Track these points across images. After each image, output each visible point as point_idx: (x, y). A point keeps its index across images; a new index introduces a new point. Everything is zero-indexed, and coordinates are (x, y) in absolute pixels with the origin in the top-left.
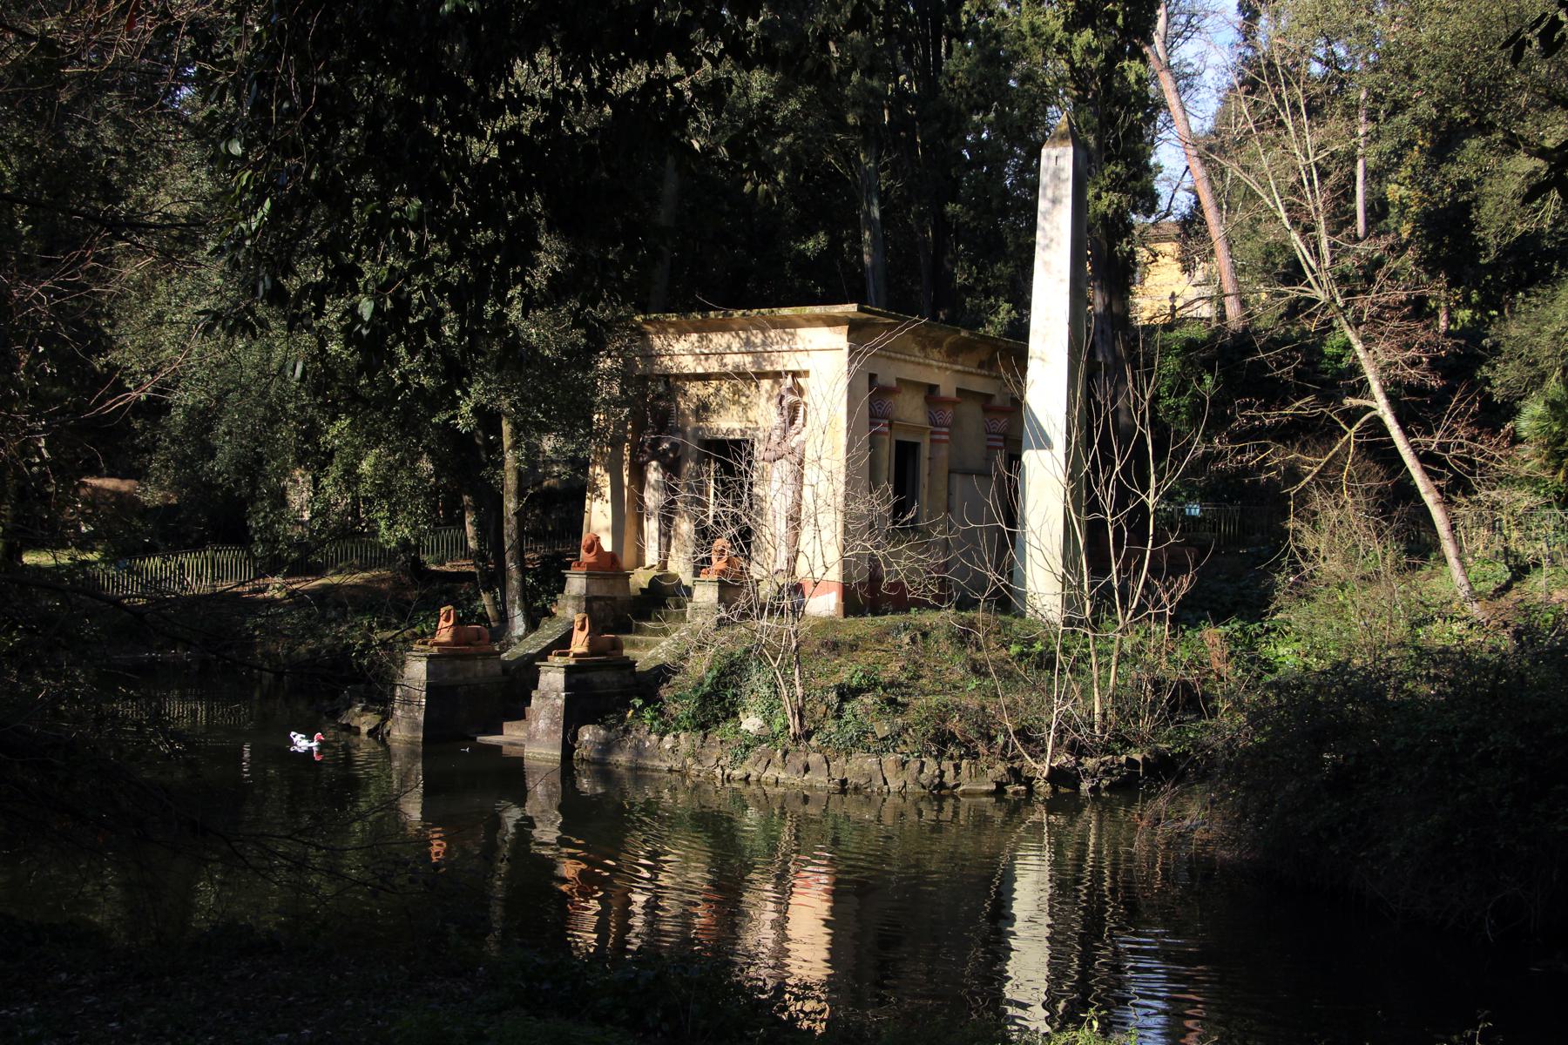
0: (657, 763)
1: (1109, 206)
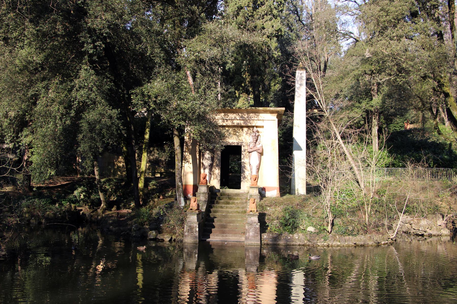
0: (294, 243)
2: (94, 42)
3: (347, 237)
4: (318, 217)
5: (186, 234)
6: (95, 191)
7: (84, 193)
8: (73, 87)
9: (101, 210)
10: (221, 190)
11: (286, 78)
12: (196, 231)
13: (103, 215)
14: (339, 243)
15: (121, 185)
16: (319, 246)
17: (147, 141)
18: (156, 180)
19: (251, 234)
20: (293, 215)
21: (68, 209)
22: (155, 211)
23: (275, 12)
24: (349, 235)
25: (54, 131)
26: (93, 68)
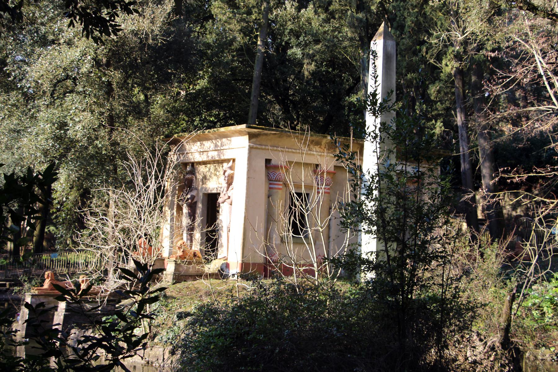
1: (452, 69)
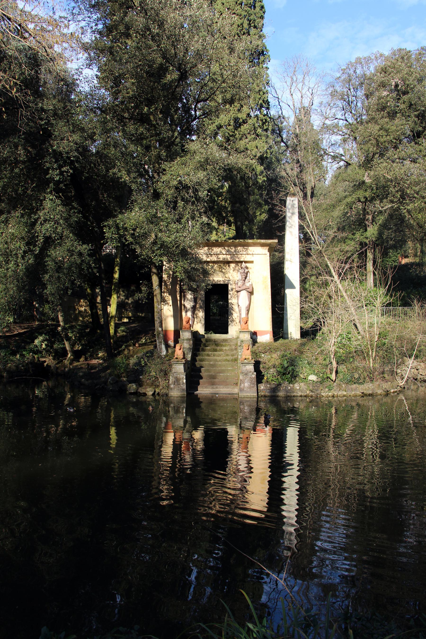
0: (295, 394)
2: (60, 167)
3: (354, 386)
4: (320, 364)
5: (172, 386)
6: (58, 339)
7: (46, 342)
8: (36, 220)
9: (68, 361)
10: (206, 335)
11: (272, 206)
12: (183, 383)
13: (71, 367)
14: (345, 393)
15: (85, 332)
16: (323, 396)
17: (117, 281)
18: (125, 326)
19: (246, 385)
20: (292, 362)
21: (31, 360)
22: (133, 361)
23: (259, 131)
24: (355, 383)
25: (15, 271)
26: (58, 197)
